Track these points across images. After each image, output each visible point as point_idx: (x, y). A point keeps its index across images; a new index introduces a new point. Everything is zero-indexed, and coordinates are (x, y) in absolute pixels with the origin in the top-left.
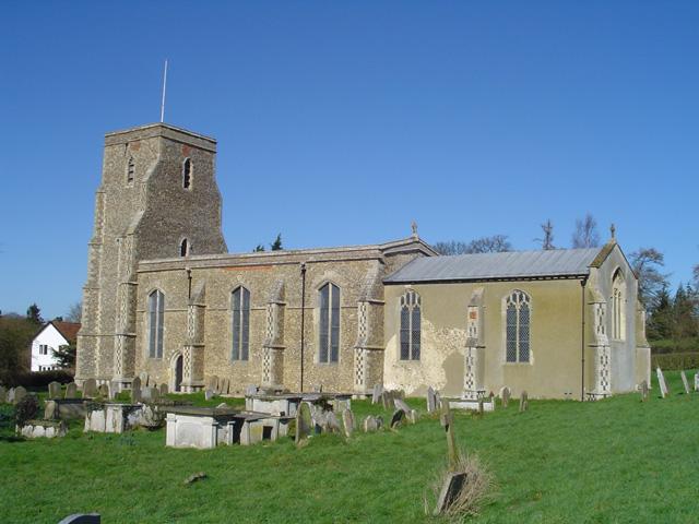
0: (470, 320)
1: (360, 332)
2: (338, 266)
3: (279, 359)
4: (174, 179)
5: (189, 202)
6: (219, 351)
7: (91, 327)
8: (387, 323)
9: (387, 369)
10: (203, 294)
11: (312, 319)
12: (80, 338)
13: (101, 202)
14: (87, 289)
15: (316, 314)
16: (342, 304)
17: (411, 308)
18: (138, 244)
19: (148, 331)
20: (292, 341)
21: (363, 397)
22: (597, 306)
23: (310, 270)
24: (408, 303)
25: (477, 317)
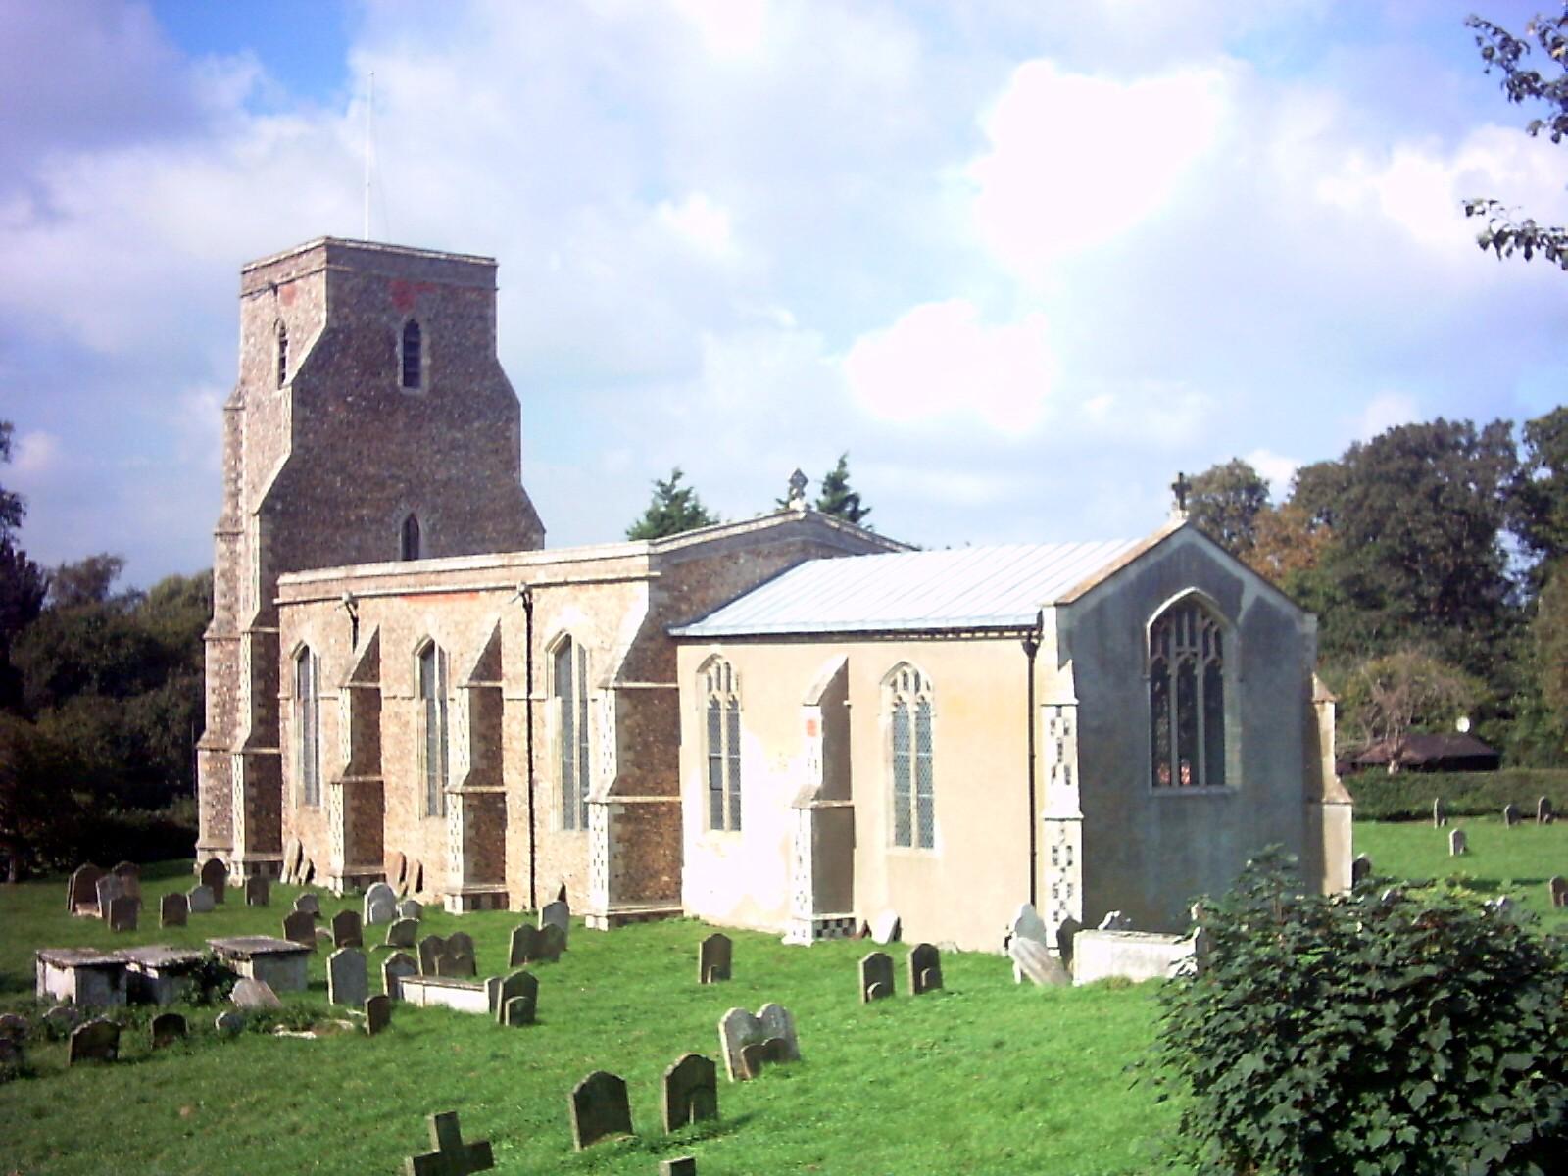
4: (371, 368)
7: (227, 731)
12: (203, 755)
18: (275, 538)
23: (540, 600)
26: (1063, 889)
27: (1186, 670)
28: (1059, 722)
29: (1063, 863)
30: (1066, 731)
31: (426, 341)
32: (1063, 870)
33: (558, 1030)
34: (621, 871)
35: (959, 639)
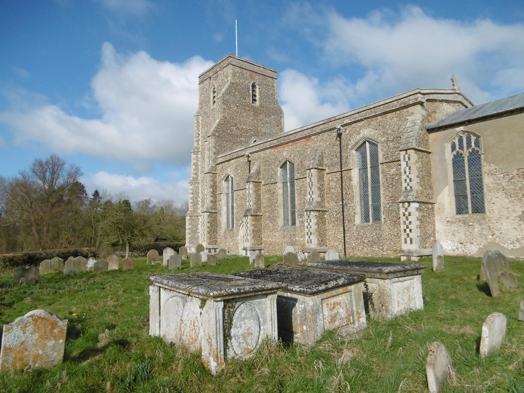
1: (404, 185)
2: (374, 122)
3: (321, 221)
5: (256, 112)
6: (273, 219)
8: (436, 173)
9: (439, 226)
10: (258, 172)
11: (351, 180)
13: (198, 122)
14: (191, 183)
15: (355, 174)
16: (381, 159)
17: (466, 153)
18: (216, 144)
19: (224, 209)
20: (333, 204)
21: (414, 259)
23: (346, 132)
24: (461, 147)
31: (257, 90)
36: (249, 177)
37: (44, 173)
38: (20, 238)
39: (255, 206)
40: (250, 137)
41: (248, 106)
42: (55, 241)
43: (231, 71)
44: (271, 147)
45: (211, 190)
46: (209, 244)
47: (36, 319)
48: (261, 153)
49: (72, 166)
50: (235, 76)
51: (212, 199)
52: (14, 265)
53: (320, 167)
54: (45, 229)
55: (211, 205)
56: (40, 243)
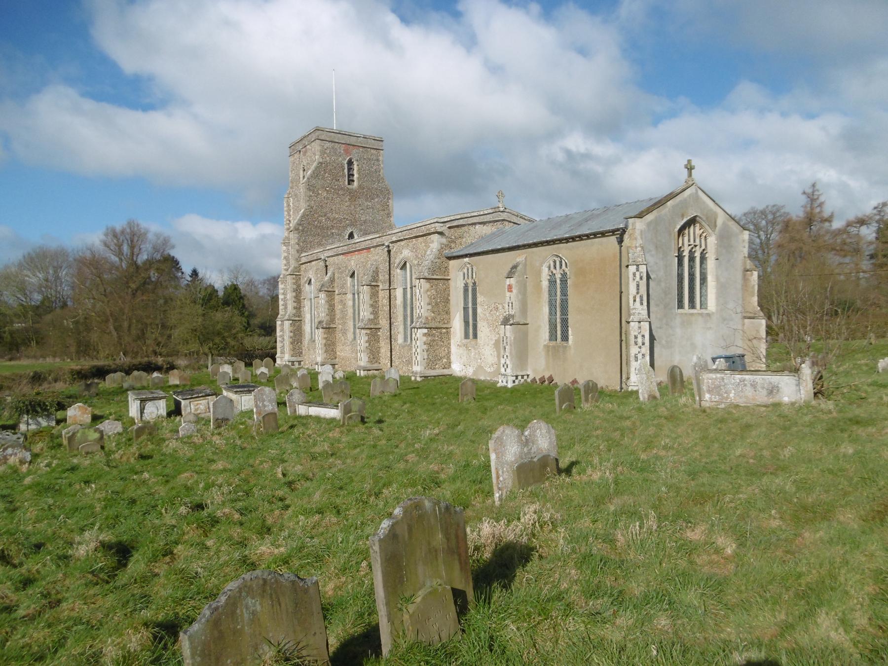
0: (508, 294)
5: (354, 196)
13: (289, 205)
17: (470, 282)
22: (632, 269)
23: (394, 248)
25: (515, 291)
26: (640, 356)
27: (691, 253)
28: (638, 274)
29: (640, 343)
30: (641, 278)
31: (355, 167)
32: (640, 347)
33: (632, 465)
34: (426, 357)
35: (582, 240)
36: (323, 286)
37: (120, 246)
38: (94, 337)
39: (328, 318)
40: (345, 228)
41: (342, 189)
42: (139, 342)
43: (319, 148)
44: (343, 254)
45: (294, 294)
46: (292, 356)
47: (79, 407)
48: (335, 258)
49: (158, 236)
50: (325, 153)
51: (295, 304)
52: (82, 378)
53: (373, 284)
54: (126, 324)
55: (294, 311)
56: (121, 344)
